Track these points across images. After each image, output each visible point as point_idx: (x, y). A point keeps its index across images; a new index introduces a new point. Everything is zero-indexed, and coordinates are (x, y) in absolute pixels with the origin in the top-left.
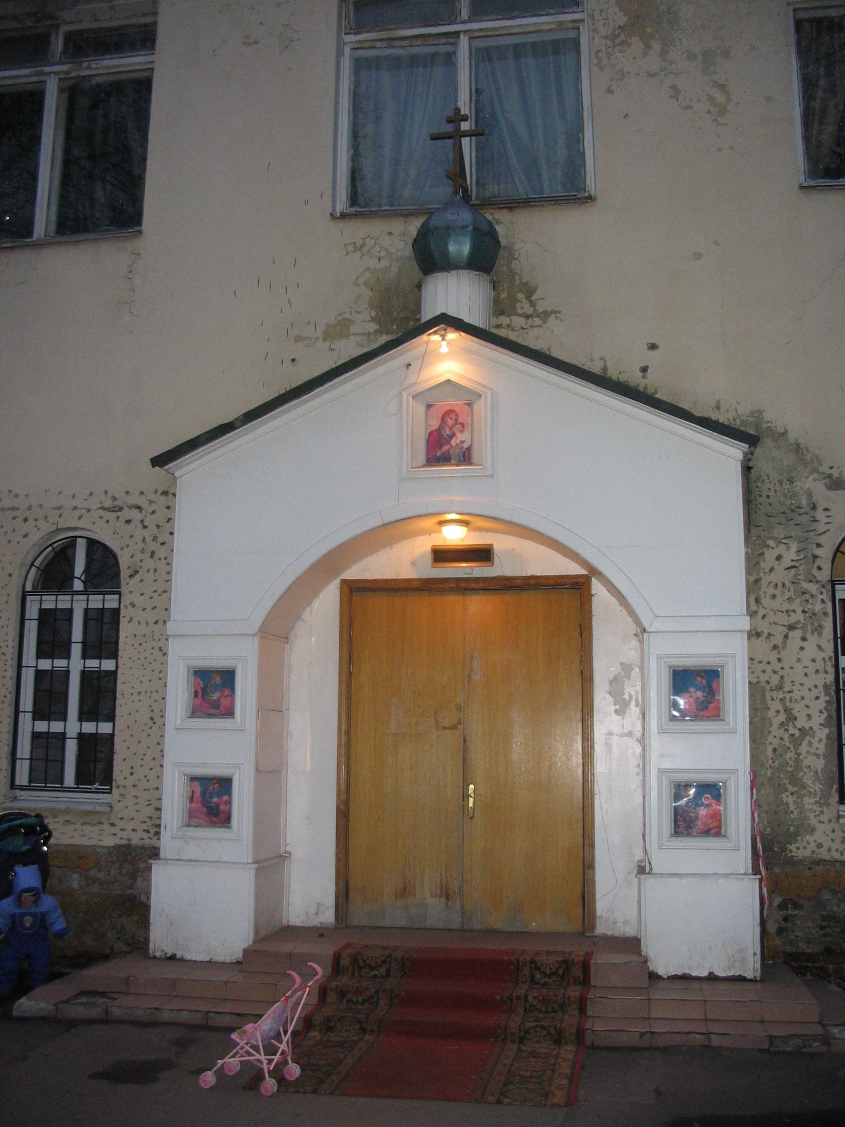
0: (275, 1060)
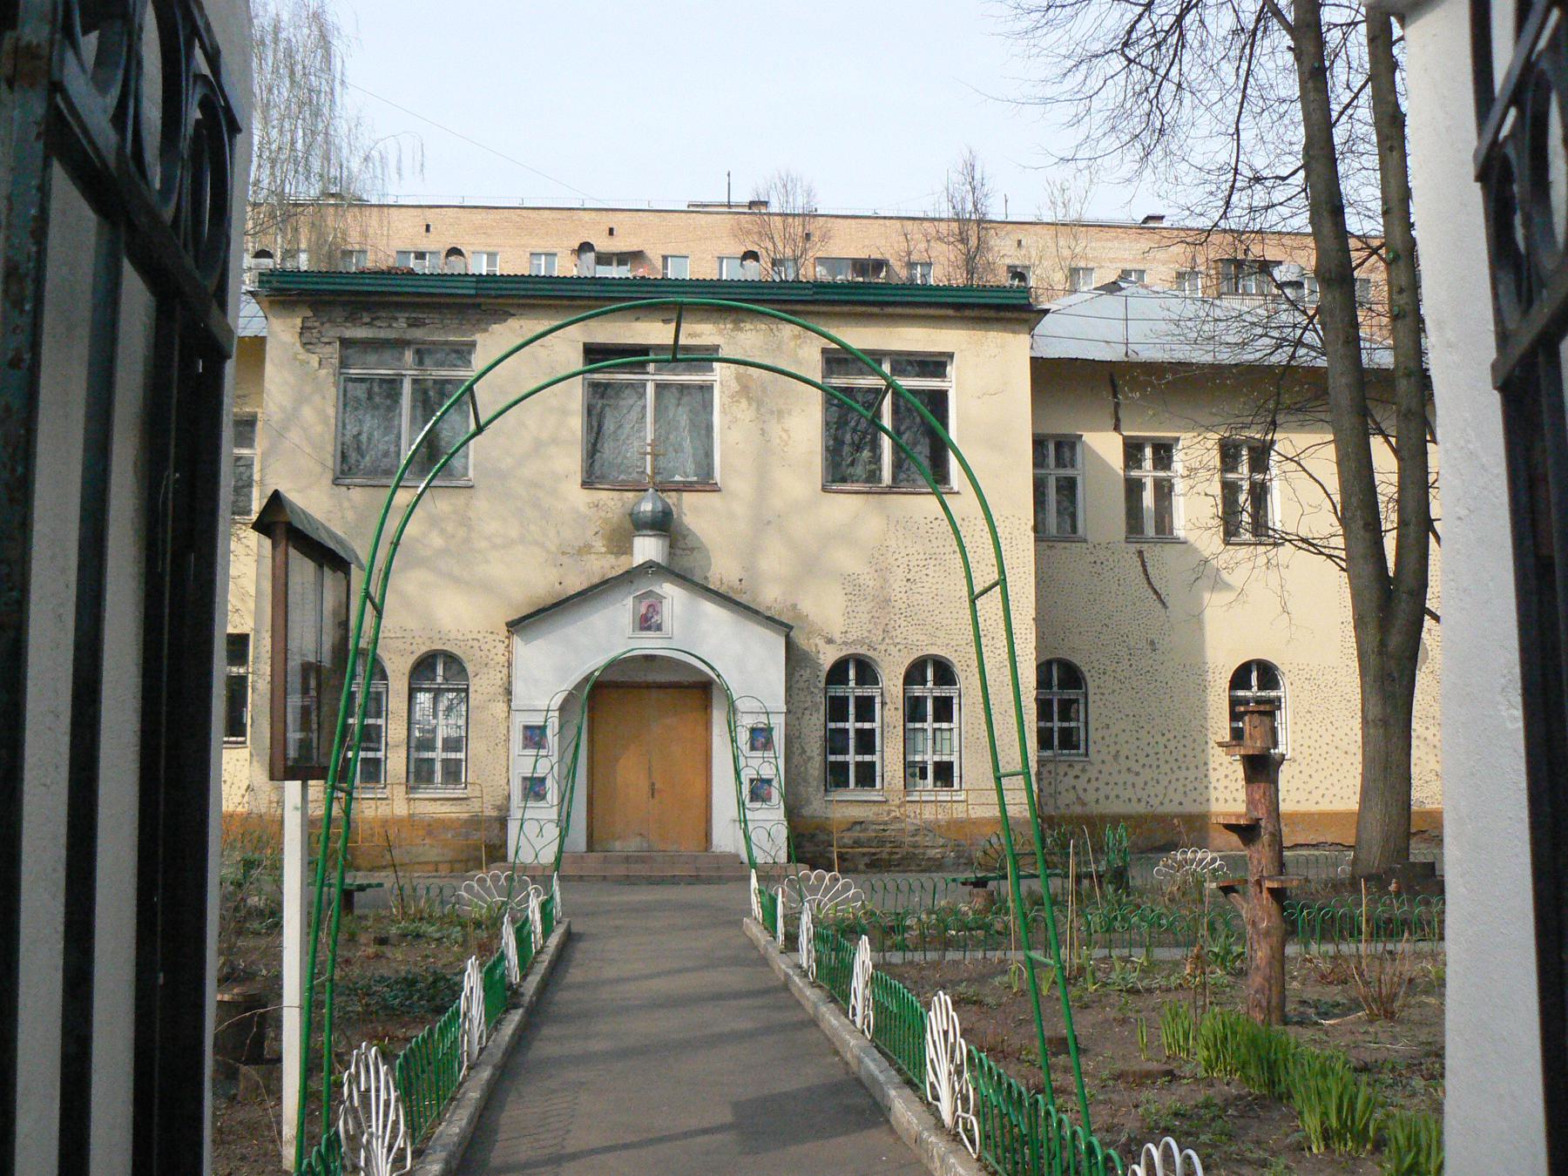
0: (830, 1017)
